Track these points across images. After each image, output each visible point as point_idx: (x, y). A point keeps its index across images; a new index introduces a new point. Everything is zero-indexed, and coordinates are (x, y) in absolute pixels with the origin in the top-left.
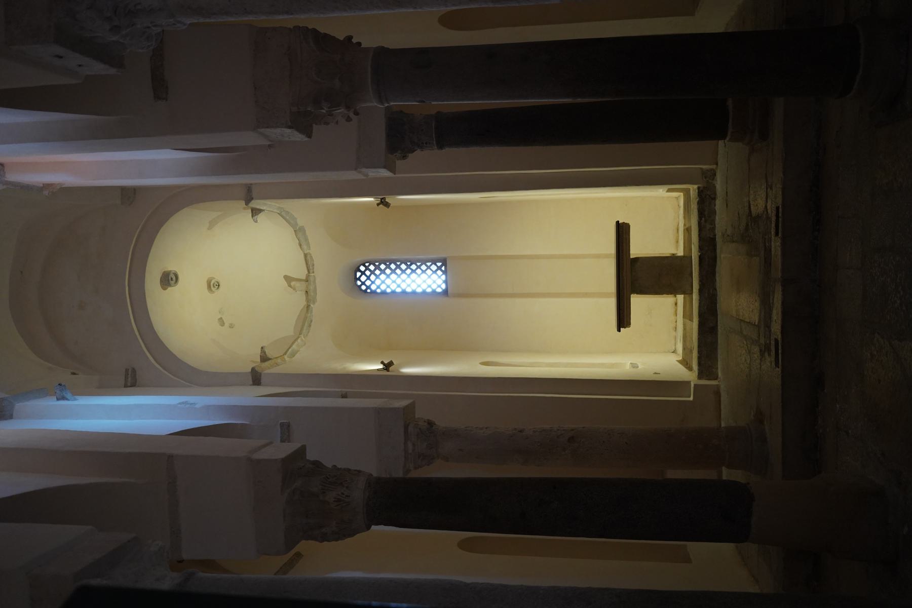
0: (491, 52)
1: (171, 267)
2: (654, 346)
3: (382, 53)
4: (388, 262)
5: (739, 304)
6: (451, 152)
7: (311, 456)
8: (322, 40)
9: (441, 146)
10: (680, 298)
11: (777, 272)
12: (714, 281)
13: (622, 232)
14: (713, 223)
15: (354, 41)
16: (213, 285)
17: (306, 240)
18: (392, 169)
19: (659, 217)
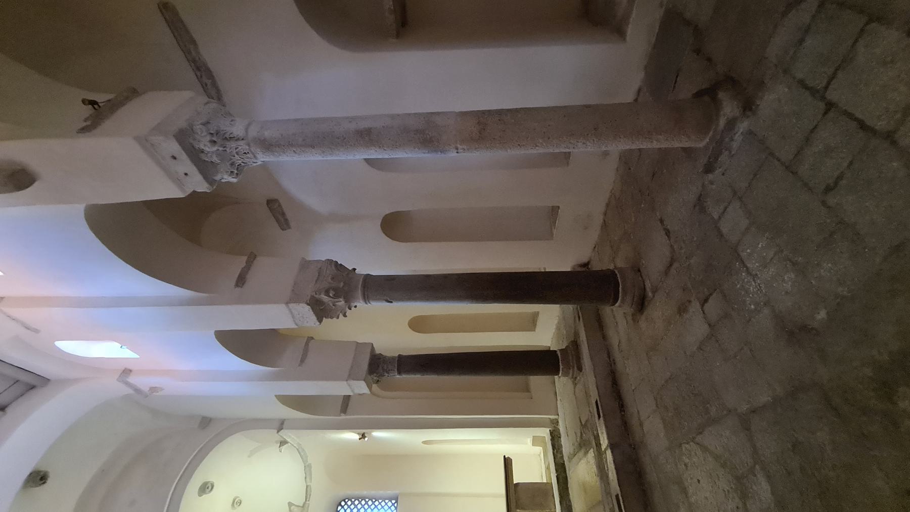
3: (368, 276)
12: (568, 494)
14: (561, 453)
17: (311, 475)
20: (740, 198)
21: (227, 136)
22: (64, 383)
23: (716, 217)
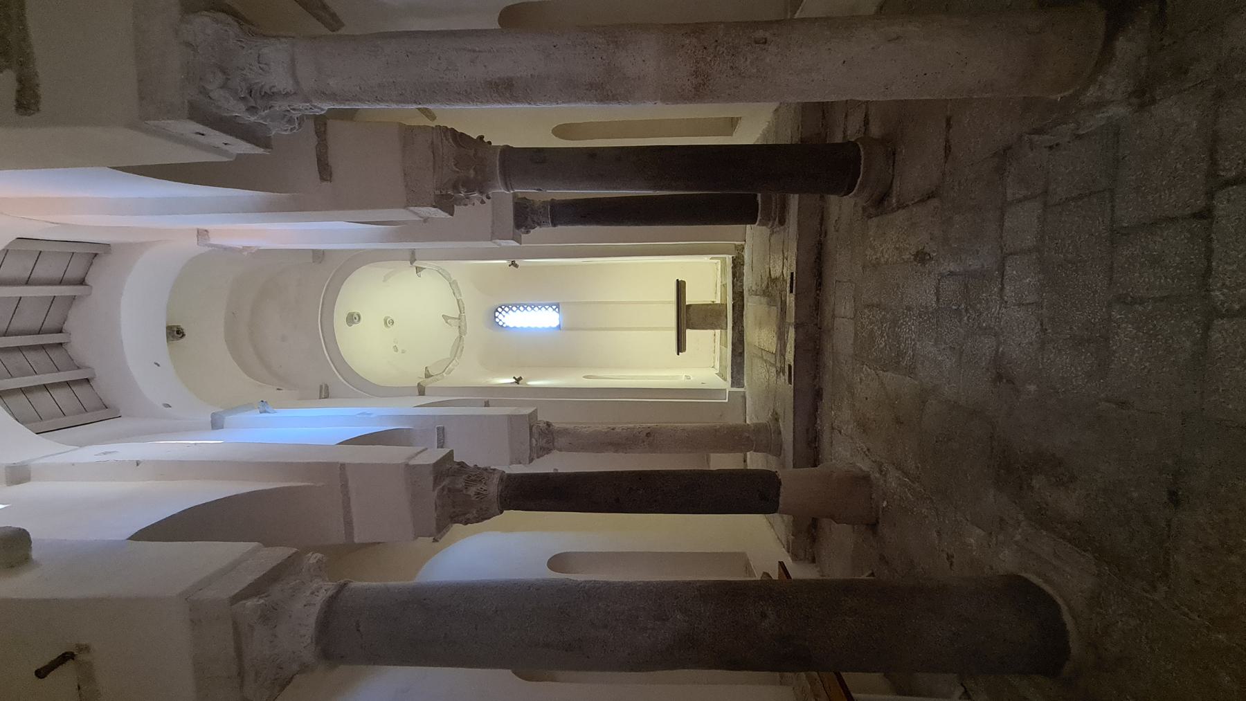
0: (592, 153)
1: (354, 310)
2: (702, 365)
3: (507, 150)
4: (518, 306)
5: (761, 336)
6: (561, 229)
7: (456, 459)
8: (459, 139)
9: (554, 225)
10: (718, 331)
11: (791, 317)
13: (680, 286)
14: (742, 281)
15: (486, 140)
16: (388, 322)
18: (519, 241)
19: (705, 275)
20: (1045, 204)
21: (266, 89)
22: (143, 246)
23: (1009, 198)
